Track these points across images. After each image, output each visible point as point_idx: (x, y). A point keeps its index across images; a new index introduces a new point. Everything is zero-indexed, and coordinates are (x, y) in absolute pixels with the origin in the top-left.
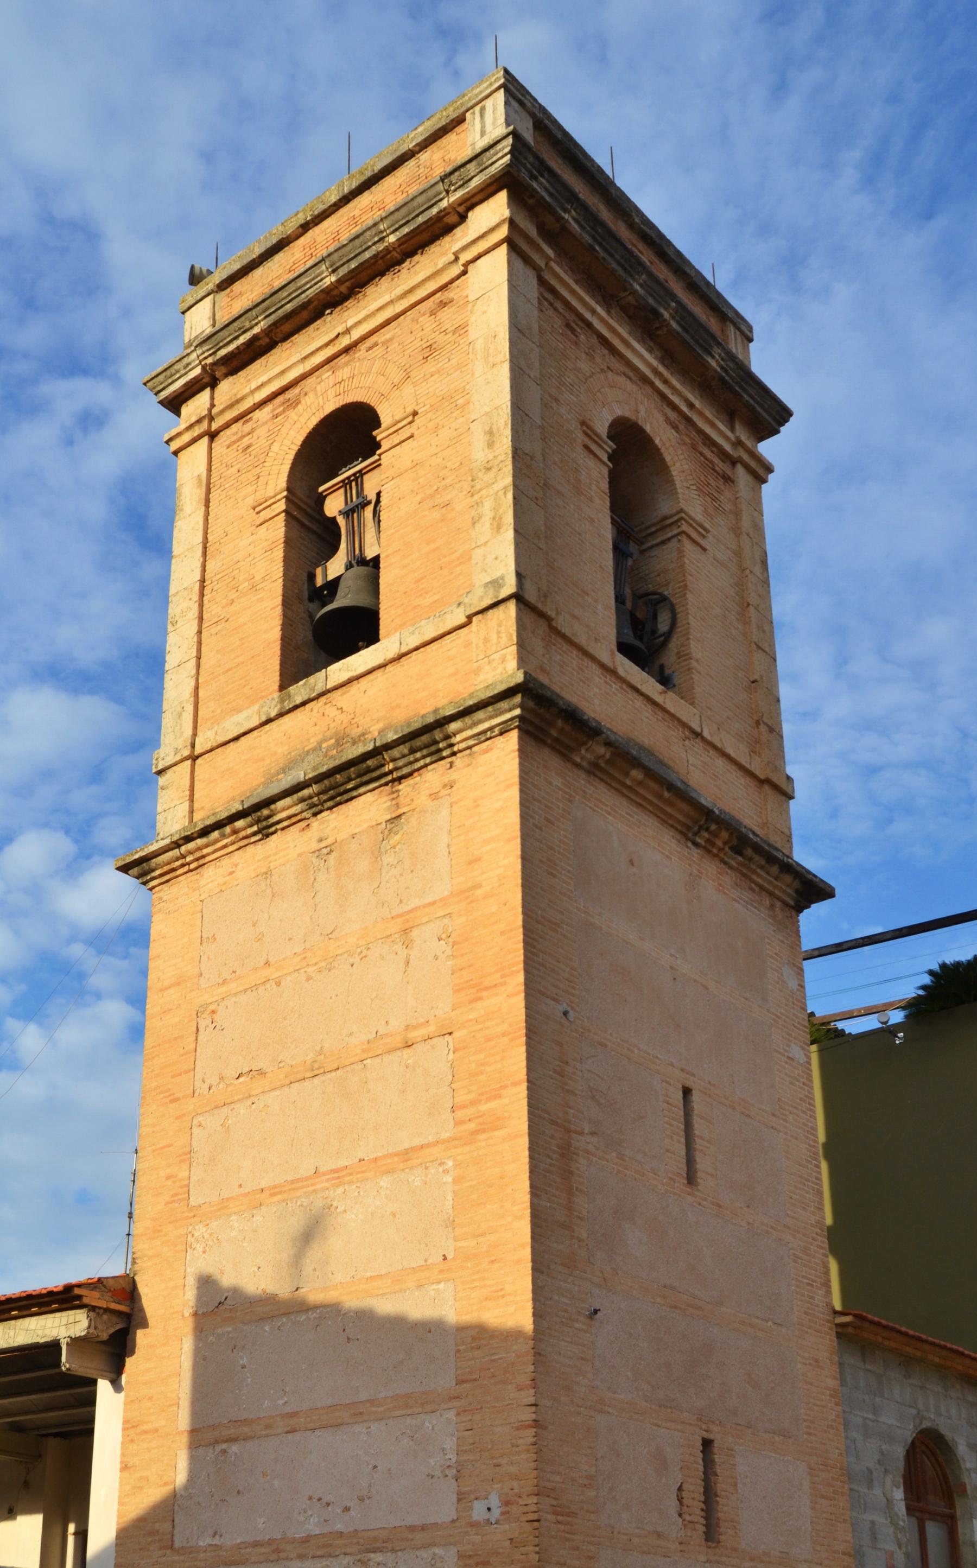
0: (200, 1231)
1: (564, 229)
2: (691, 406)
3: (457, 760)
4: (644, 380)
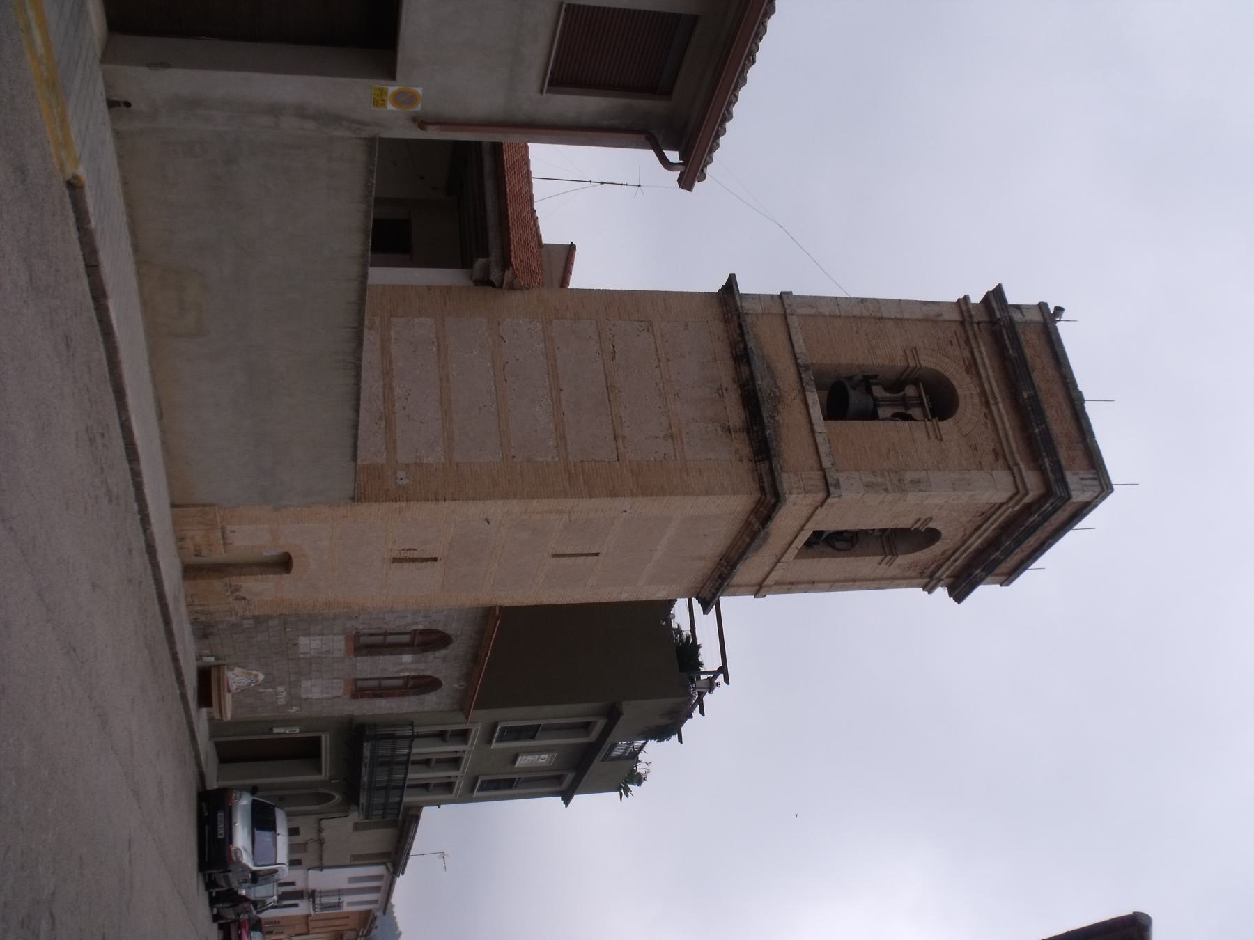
0: (539, 326)
1: (1031, 514)
2: (955, 561)
3: (751, 464)
4: (964, 542)
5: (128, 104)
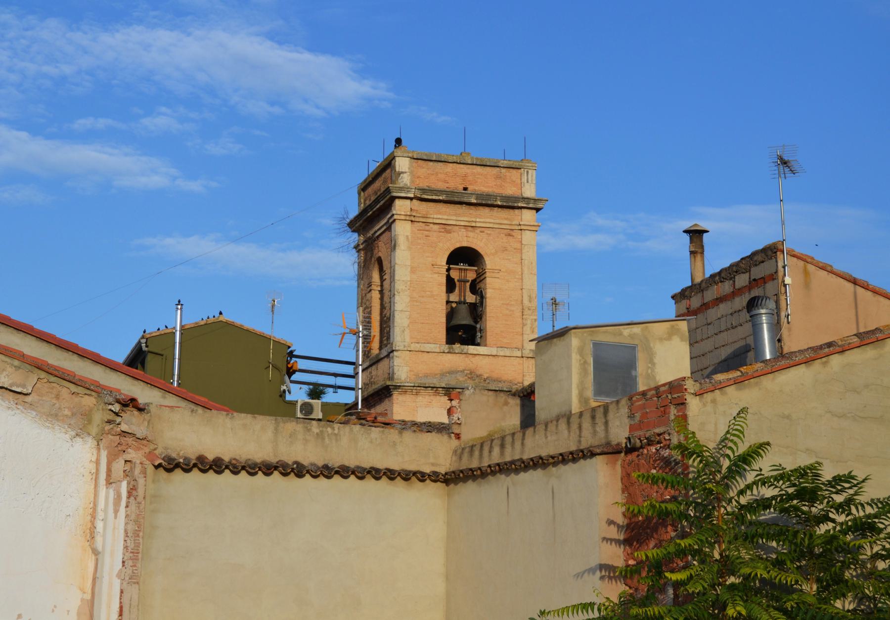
5: (768, 444)
